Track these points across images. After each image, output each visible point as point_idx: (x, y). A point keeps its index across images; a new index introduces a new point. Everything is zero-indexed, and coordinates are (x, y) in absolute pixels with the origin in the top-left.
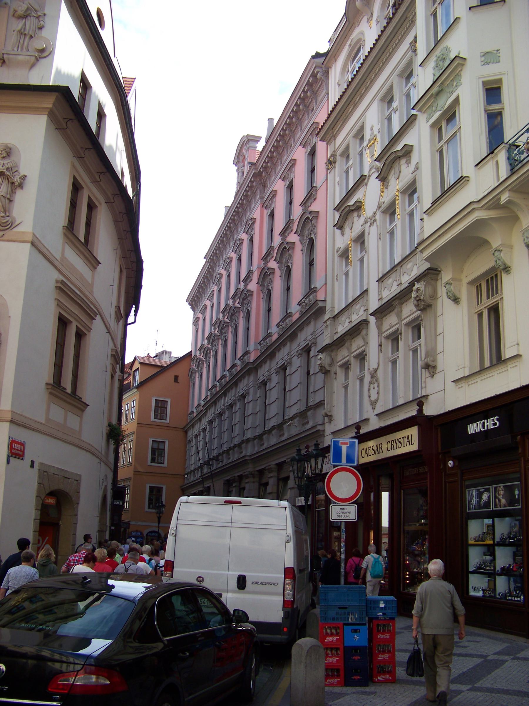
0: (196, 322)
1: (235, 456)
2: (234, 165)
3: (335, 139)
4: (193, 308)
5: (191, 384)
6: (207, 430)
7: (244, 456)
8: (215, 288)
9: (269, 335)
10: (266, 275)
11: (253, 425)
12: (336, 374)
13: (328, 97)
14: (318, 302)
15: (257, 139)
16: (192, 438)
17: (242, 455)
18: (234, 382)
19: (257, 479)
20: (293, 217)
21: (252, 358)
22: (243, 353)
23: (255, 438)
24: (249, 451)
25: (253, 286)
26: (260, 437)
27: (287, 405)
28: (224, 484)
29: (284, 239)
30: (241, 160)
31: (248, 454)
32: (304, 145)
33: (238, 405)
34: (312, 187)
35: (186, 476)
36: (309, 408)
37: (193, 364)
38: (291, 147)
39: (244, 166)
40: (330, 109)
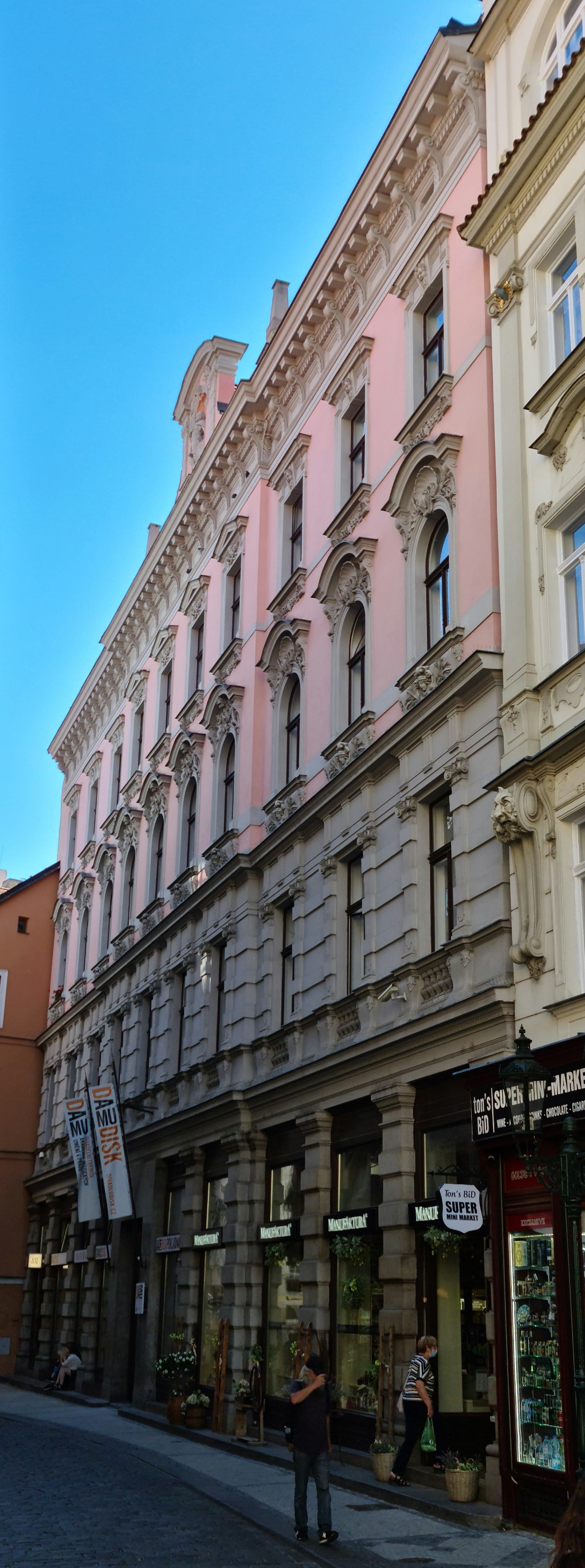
0: (71, 795)
1: (193, 1096)
2: (176, 423)
3: (516, 232)
4: (64, 768)
5: (59, 936)
6: (104, 1040)
7: (229, 1093)
8: (128, 708)
9: (294, 784)
10: (285, 638)
11: (252, 1011)
12: (552, 840)
13: (484, 142)
14: (481, 656)
15: (236, 350)
16: (60, 1061)
17: (218, 1092)
18: (158, 939)
19: (261, 1154)
20: (203, 685)
21: (246, 844)
22: (148, 904)
23: (256, 1046)
24: (242, 1076)
25: (244, 674)
26: (277, 1041)
27: (184, 1046)
28: (157, 1169)
29: (185, 725)
30: (194, 406)
31: (239, 1087)
32: (334, 397)
33: (166, 992)
34: (234, 639)
35: (41, 1154)
36: (219, 1057)
37: (65, 889)
38: (209, 538)
39: (203, 418)
40: (493, 169)
